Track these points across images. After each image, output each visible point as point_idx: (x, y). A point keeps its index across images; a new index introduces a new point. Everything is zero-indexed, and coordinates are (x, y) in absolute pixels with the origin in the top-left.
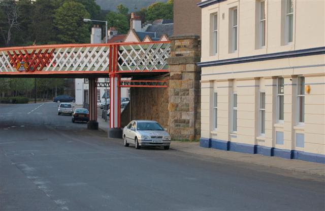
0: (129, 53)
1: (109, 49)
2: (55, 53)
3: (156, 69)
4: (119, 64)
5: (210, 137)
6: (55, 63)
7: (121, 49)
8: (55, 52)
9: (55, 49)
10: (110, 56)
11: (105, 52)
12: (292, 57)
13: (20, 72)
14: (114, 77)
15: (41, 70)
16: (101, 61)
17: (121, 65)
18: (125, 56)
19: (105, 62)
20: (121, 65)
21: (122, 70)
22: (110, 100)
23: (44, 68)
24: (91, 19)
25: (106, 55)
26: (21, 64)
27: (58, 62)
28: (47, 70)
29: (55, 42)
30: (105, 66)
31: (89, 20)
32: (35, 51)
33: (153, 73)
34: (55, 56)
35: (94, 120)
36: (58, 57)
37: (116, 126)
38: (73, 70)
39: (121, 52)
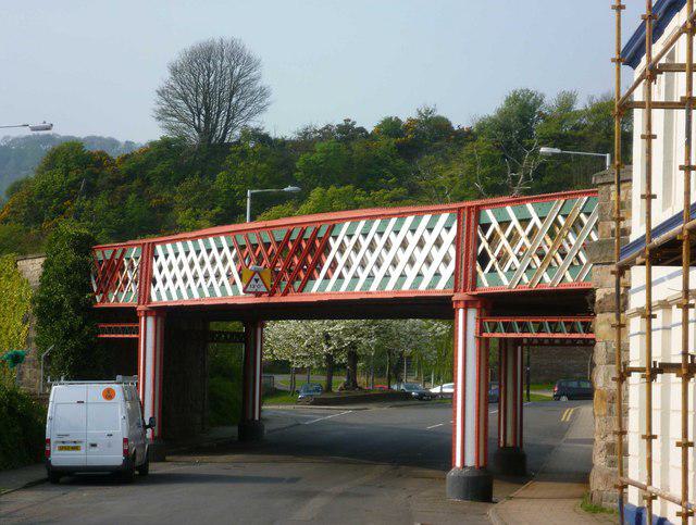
0: (524, 228)
1: (456, 223)
2: (335, 238)
3: (569, 279)
4: (478, 268)
5: (662, 512)
6: (334, 264)
7: (483, 221)
8: (334, 234)
9: (334, 225)
10: (457, 242)
11: (448, 229)
12: (646, 124)
13: (259, 294)
14: (466, 309)
15: (301, 290)
16: (438, 256)
17: (483, 269)
18: (493, 240)
19: (446, 261)
20: (483, 269)
21: (486, 285)
22: (261, 357)
23: (310, 282)
24: (560, 147)
25: (449, 237)
26: (256, 272)
27: (341, 261)
28: (314, 290)
29: (88, 148)
30: (447, 273)
31: (557, 151)
32: (290, 233)
33: (518, 293)
34: (335, 245)
35: (514, 447)
36: (341, 249)
37: (470, 462)
38: (374, 288)
39: (485, 227)
